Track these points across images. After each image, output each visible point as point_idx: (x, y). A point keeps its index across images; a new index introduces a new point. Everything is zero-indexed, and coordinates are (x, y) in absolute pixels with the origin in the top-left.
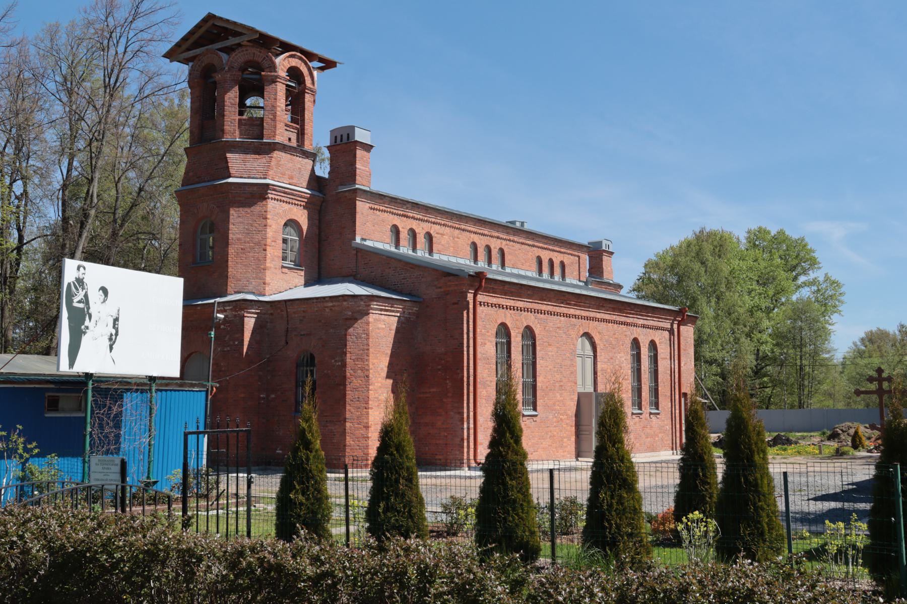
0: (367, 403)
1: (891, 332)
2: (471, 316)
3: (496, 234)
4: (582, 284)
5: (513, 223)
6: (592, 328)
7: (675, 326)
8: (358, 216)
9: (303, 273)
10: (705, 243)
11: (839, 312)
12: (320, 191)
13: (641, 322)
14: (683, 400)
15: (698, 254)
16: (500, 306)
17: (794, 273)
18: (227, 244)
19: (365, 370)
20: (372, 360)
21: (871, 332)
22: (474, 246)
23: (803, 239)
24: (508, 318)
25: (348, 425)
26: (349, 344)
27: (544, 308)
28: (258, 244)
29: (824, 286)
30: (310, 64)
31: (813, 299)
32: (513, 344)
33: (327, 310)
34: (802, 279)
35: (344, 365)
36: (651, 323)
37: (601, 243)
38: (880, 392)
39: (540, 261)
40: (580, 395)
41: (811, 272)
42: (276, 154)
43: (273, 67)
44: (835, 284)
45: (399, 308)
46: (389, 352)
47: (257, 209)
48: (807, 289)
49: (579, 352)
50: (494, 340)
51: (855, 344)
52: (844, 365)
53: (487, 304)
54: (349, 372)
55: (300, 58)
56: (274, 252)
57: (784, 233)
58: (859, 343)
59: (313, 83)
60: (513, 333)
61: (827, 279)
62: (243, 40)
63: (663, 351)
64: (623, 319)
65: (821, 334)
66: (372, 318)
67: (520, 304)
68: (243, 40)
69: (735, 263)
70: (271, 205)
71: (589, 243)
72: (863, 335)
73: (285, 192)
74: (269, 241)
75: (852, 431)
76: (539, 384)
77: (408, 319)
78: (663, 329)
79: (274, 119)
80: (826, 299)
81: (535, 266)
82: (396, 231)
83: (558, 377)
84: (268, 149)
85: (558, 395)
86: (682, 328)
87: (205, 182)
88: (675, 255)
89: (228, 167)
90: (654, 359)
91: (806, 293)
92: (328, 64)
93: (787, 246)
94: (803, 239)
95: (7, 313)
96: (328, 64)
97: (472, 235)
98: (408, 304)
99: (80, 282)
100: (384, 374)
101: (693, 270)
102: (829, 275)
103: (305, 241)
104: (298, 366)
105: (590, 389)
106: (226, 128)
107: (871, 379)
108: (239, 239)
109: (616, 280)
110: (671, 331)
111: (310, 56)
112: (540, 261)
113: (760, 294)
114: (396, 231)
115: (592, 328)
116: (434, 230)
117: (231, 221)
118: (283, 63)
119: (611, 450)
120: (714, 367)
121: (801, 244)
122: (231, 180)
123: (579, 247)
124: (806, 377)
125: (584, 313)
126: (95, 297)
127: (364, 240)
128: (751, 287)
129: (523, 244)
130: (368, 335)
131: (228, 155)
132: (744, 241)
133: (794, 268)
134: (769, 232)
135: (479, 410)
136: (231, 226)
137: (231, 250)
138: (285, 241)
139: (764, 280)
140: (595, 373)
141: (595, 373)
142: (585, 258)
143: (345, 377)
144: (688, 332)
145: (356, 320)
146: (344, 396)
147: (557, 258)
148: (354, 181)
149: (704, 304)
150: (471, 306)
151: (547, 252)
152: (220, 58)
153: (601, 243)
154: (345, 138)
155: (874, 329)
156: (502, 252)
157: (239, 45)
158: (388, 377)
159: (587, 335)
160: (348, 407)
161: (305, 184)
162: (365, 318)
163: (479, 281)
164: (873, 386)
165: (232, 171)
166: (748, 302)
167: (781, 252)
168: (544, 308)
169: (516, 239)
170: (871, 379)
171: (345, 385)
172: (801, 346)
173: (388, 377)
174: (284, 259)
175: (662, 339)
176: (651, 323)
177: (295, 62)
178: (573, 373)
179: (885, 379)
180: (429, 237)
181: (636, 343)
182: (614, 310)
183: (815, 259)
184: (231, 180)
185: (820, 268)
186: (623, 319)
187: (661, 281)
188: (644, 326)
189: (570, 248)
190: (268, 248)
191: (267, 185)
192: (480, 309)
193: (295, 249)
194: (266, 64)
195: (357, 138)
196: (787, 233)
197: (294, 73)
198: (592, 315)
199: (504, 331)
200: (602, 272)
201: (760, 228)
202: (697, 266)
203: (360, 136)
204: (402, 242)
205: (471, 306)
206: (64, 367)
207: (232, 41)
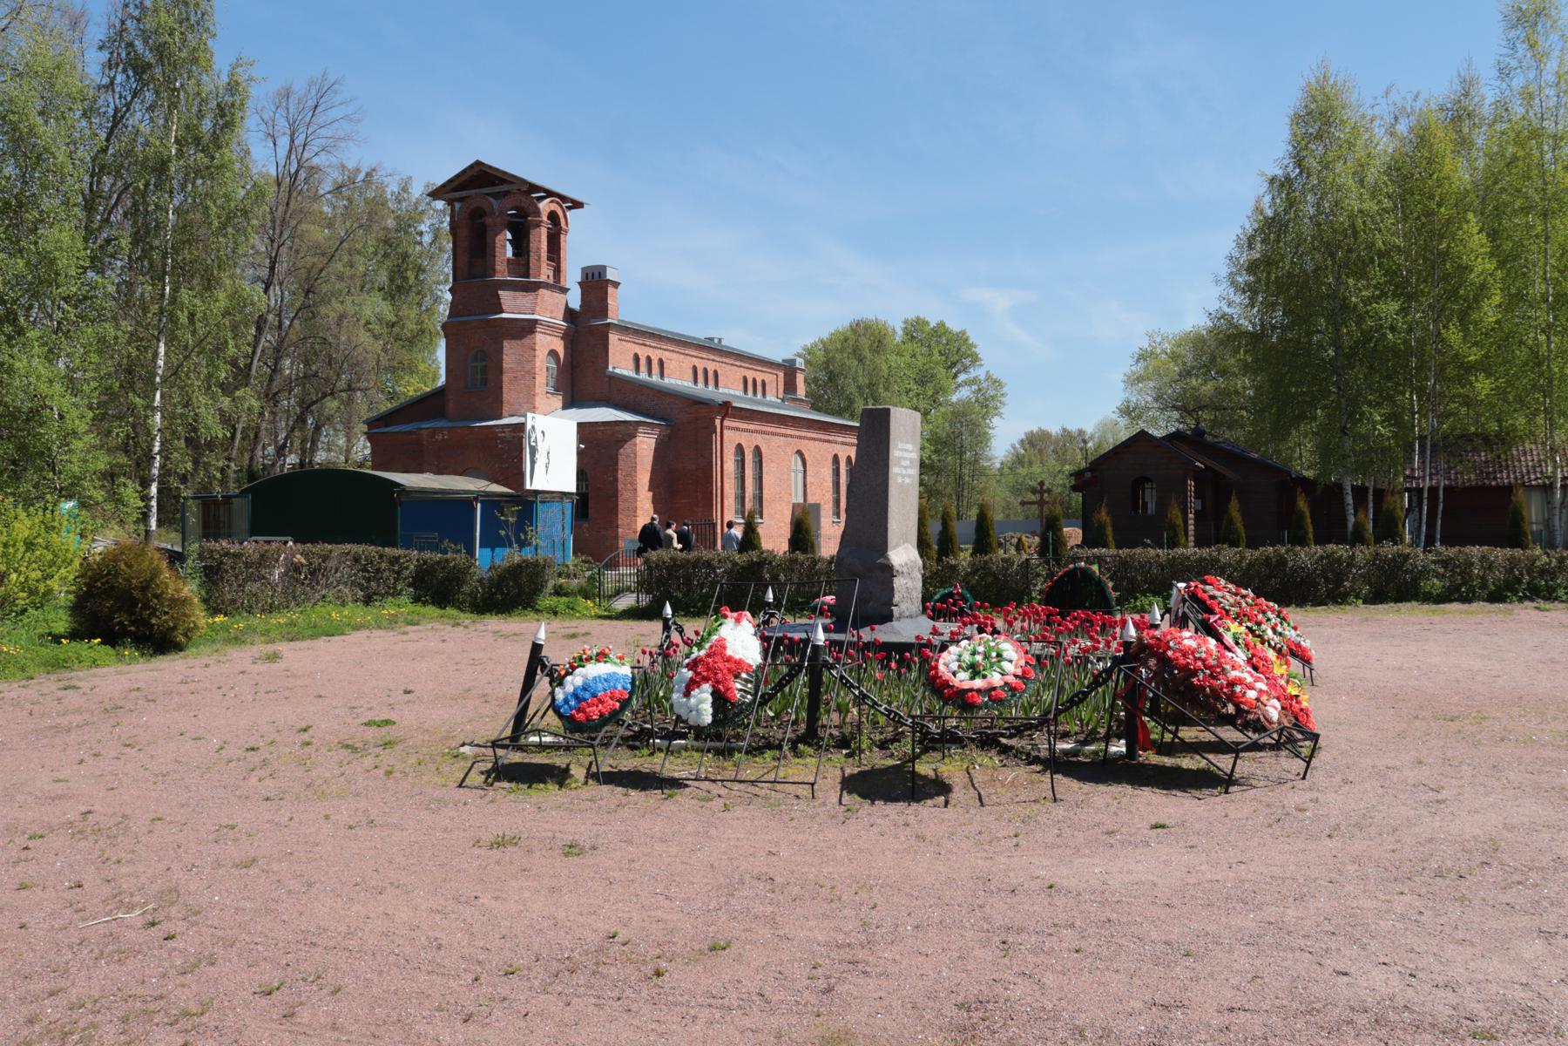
0: (635, 512)
1: (1054, 434)
2: (719, 438)
3: (712, 357)
4: (779, 401)
5: (711, 339)
8: (610, 347)
9: (561, 397)
10: (863, 338)
11: (1000, 415)
12: (572, 323)
13: (840, 439)
15: (855, 351)
16: (737, 429)
17: (954, 371)
18: (501, 373)
19: (634, 484)
20: (639, 476)
21: (1032, 432)
22: (695, 369)
23: (964, 333)
25: (620, 530)
26: (620, 462)
27: (769, 429)
28: (528, 372)
29: (984, 385)
30: (564, 205)
31: (973, 400)
32: (746, 461)
33: (599, 433)
34: (962, 377)
35: (616, 480)
38: (1041, 503)
40: (794, 504)
41: (971, 370)
42: (542, 292)
43: (538, 213)
44: (997, 383)
45: (657, 431)
46: (650, 469)
47: (526, 341)
48: (967, 388)
49: (793, 467)
51: (1013, 447)
52: (1001, 470)
53: (733, 429)
54: (620, 486)
55: (558, 203)
58: (1018, 446)
59: (567, 224)
60: (746, 453)
62: (513, 188)
64: (827, 437)
65: (981, 439)
66: (638, 440)
67: (752, 427)
68: (513, 188)
69: (893, 358)
71: (784, 361)
72: (1023, 437)
73: (550, 326)
74: (537, 370)
75: (1015, 541)
76: (764, 496)
77: (662, 440)
80: (987, 400)
81: (742, 386)
84: (533, 287)
87: (475, 315)
89: (500, 304)
91: (965, 393)
92: (577, 205)
93: (947, 340)
94: (964, 333)
95: (1508, 551)
96: (577, 205)
97: (694, 359)
98: (664, 428)
99: (533, 427)
100: (647, 488)
102: (991, 373)
103: (560, 369)
105: (801, 500)
106: (497, 267)
107: (1034, 491)
108: (512, 368)
111: (563, 198)
113: (918, 395)
115: (805, 446)
116: (665, 355)
117: (505, 352)
118: (545, 206)
121: (961, 338)
124: (966, 487)
125: (797, 433)
127: (614, 368)
128: (908, 386)
129: (732, 365)
130: (635, 454)
131: (500, 292)
132: (900, 333)
133: (954, 364)
134: (927, 323)
136: (505, 357)
137: (505, 378)
140: (805, 486)
141: (805, 486)
142: (781, 375)
143: (617, 490)
145: (626, 442)
146: (617, 506)
148: (606, 316)
150: (718, 430)
154: (596, 275)
155: (1035, 429)
157: (508, 192)
158: (649, 490)
159: (799, 453)
160: (620, 516)
161: (561, 318)
162: (633, 440)
164: (1033, 498)
165: (504, 307)
167: (941, 347)
168: (769, 429)
169: (727, 360)
170: (1034, 491)
171: (617, 497)
172: (961, 454)
173: (649, 490)
177: (554, 207)
178: (789, 486)
179: (1045, 492)
180: (661, 363)
182: (820, 429)
183: (977, 355)
184: (504, 315)
185: (981, 365)
186: (827, 437)
188: (843, 443)
189: (770, 367)
190: (537, 376)
192: (725, 431)
194: (531, 209)
195: (609, 277)
196: (947, 325)
197: (553, 217)
198: (803, 434)
199: (740, 449)
200: (796, 389)
201: (918, 318)
203: (611, 275)
205: (718, 430)
207: (505, 188)
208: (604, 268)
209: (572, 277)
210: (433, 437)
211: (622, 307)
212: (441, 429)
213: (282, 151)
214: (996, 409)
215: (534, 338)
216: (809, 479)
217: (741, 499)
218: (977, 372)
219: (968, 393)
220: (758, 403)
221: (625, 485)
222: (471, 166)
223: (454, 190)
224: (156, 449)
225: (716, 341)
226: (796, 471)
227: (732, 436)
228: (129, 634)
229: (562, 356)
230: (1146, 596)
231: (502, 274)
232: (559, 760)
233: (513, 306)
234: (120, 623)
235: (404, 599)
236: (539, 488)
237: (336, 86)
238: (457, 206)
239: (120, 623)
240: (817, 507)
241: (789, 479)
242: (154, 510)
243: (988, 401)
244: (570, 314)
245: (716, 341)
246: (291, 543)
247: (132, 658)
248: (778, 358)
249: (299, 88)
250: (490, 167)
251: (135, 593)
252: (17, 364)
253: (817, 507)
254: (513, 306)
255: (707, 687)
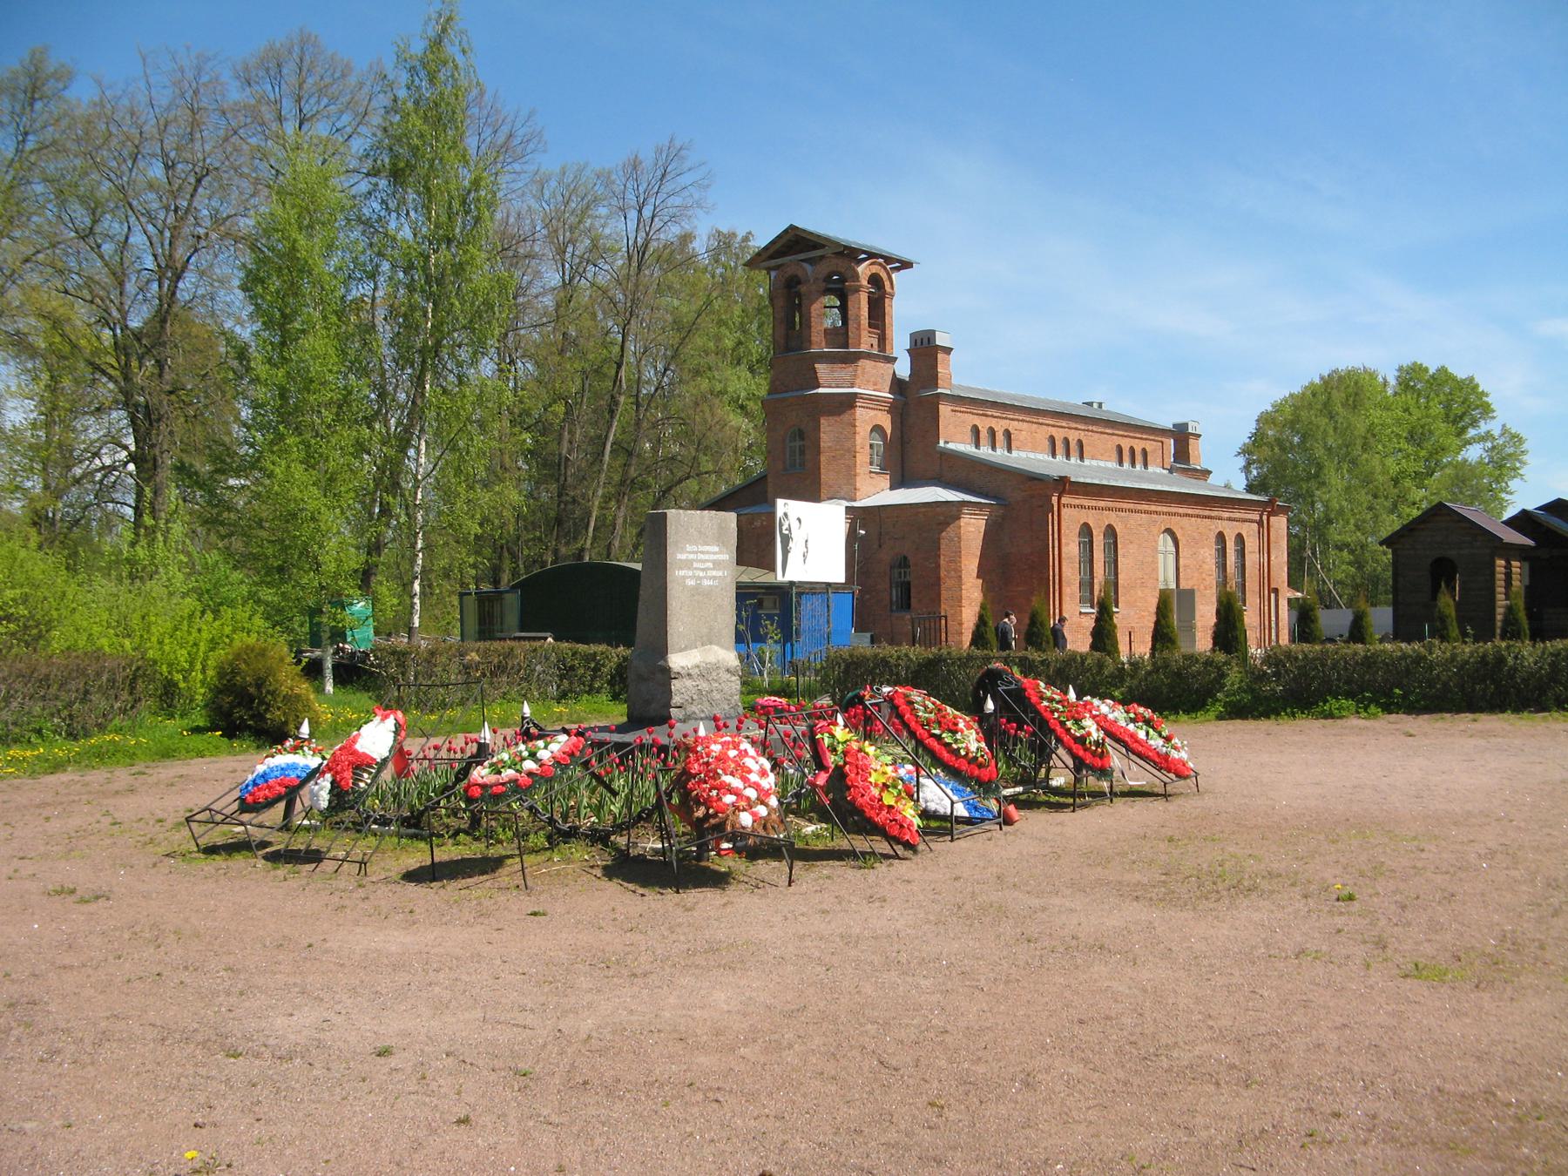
3: (1074, 425)
4: (1166, 472)
6: (1176, 524)
7: (1265, 517)
12: (901, 394)
13: (1226, 515)
14: (1273, 595)
18: (819, 453)
19: (958, 571)
22: (1052, 440)
23: (1471, 379)
24: (1091, 518)
26: (942, 547)
27: (1125, 506)
28: (849, 450)
34: (1471, 432)
35: (938, 566)
36: (1237, 515)
37: (1186, 425)
39: (1120, 450)
42: (863, 363)
43: (856, 277)
44: (1516, 439)
47: (846, 417)
50: (1077, 540)
54: (943, 573)
55: (880, 264)
56: (862, 458)
57: (1446, 371)
59: (892, 287)
61: (1504, 430)
63: (1251, 544)
64: (1207, 513)
67: (1102, 504)
70: (859, 411)
71: (1174, 426)
73: (871, 399)
74: (858, 448)
78: (1252, 521)
79: (858, 328)
80: (1504, 459)
81: (1115, 455)
82: (976, 431)
83: (1139, 574)
85: (1139, 593)
86: (1272, 519)
88: (1296, 408)
90: (1241, 553)
92: (906, 265)
94: (1471, 379)
96: (906, 265)
97: (1050, 428)
99: (786, 514)
101: (1318, 427)
104: (892, 568)
109: (1203, 464)
110: (1260, 523)
112: (1120, 450)
114: (976, 431)
115: (1176, 524)
116: (1013, 426)
118: (864, 270)
119: (1163, 622)
120: (1345, 553)
121: (1469, 386)
122: (821, 390)
123: (1163, 432)
125: (1165, 509)
126: (794, 525)
127: (946, 442)
132: (1392, 382)
134: (1426, 370)
135: (1064, 607)
137: (823, 458)
138: (871, 446)
139: (1416, 436)
143: (939, 578)
144: (1280, 523)
145: (948, 524)
147: (1139, 446)
148: (936, 386)
149: (1333, 472)
150: (1056, 509)
151: (1128, 440)
152: (804, 269)
153: (1186, 425)
154: (925, 341)
156: (1080, 444)
157: (822, 257)
159: (1169, 531)
163: (1064, 485)
166: (1393, 466)
169: (1094, 428)
173: (978, 577)
174: (871, 464)
175: (1250, 532)
176: (1237, 515)
178: (1155, 570)
180: (1008, 434)
181: (1221, 537)
184: (821, 390)
185: (1494, 418)
186: (1207, 513)
187: (1279, 442)
191: (856, 394)
192: (1064, 511)
193: (881, 453)
195: (939, 342)
196: (1450, 370)
199: (1086, 531)
202: (1323, 421)
203: (940, 340)
204: (982, 441)
205: (1056, 509)
206: (780, 578)
207: (818, 253)
208: (933, 332)
209: (900, 345)
210: (752, 523)
211: (958, 374)
212: (759, 514)
213: (632, 225)
214: (1515, 469)
215: (854, 414)
216: (1181, 561)
217: (1087, 584)
218: (1491, 426)
219: (1481, 451)
220: (1140, 478)
221: (948, 572)
222: (786, 231)
223: (772, 257)
224: (419, 546)
225: (1095, 406)
226: (1165, 553)
227: (1072, 516)
228: (249, 727)
229: (889, 432)
230: (1337, 699)
231: (819, 345)
232: (318, 843)
233: (831, 381)
234: (241, 717)
235: (604, 697)
236: (796, 579)
237: (683, 152)
238: (773, 274)
239: (241, 717)
240: (1190, 593)
241: (1155, 562)
242: (418, 607)
243: (1505, 461)
244: (897, 385)
245: (1095, 406)
246: (550, 640)
247: (246, 751)
248: (1168, 424)
249: (648, 158)
250: (804, 231)
251: (252, 690)
252: (278, 470)
253: (1190, 593)
254: (831, 381)
255: (328, 776)
